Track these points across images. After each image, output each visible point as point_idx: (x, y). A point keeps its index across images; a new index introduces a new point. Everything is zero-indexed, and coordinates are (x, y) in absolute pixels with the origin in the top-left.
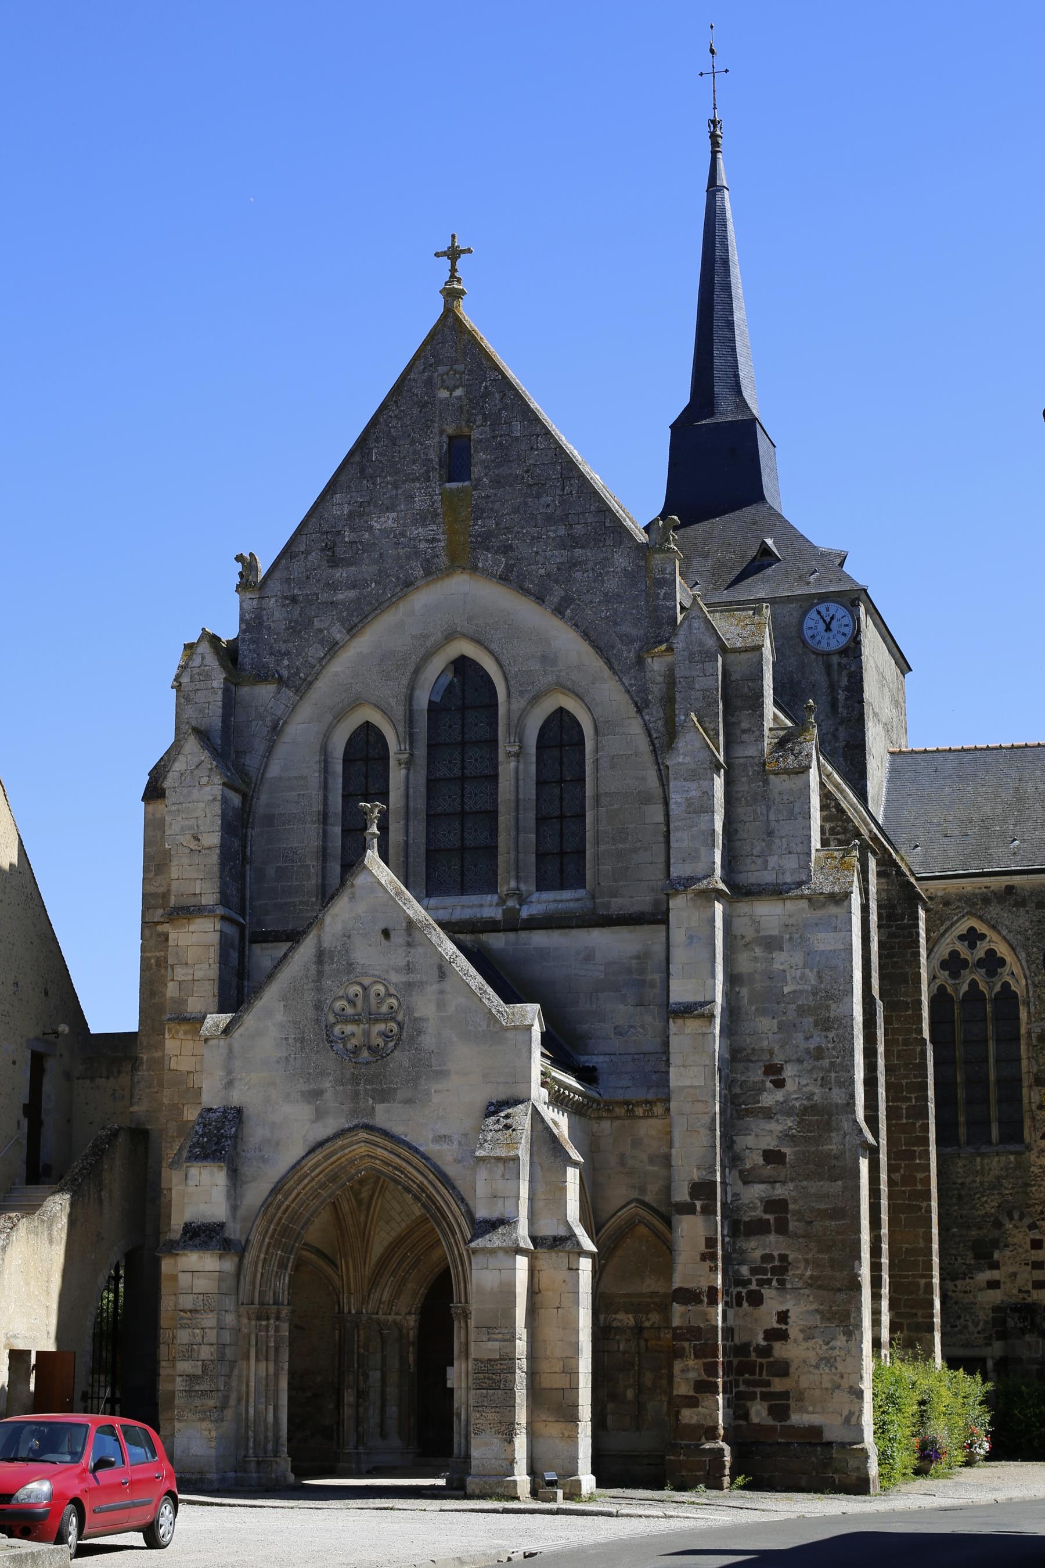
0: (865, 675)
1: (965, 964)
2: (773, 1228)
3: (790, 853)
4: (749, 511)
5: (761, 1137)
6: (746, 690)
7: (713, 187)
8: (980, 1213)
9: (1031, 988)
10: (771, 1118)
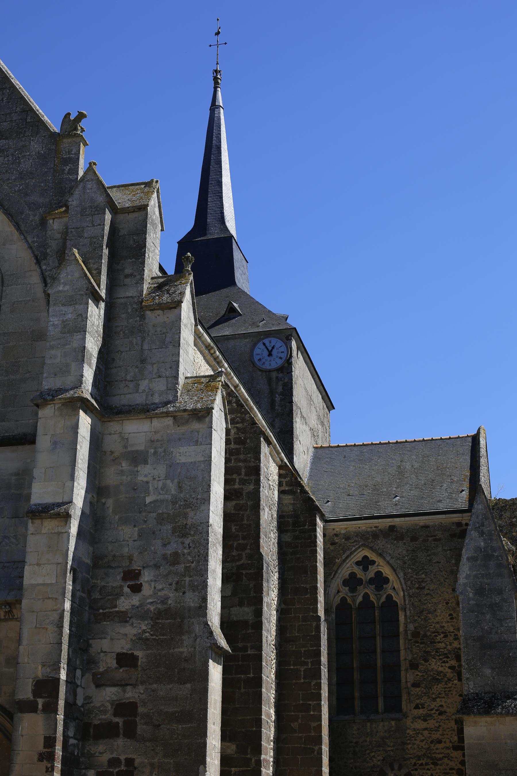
0: (294, 386)
1: (360, 582)
2: (121, 731)
3: (160, 377)
4: (225, 291)
5: (115, 641)
6: (131, 242)
7: (214, 106)
8: (369, 764)
9: (407, 598)
10: (126, 622)
